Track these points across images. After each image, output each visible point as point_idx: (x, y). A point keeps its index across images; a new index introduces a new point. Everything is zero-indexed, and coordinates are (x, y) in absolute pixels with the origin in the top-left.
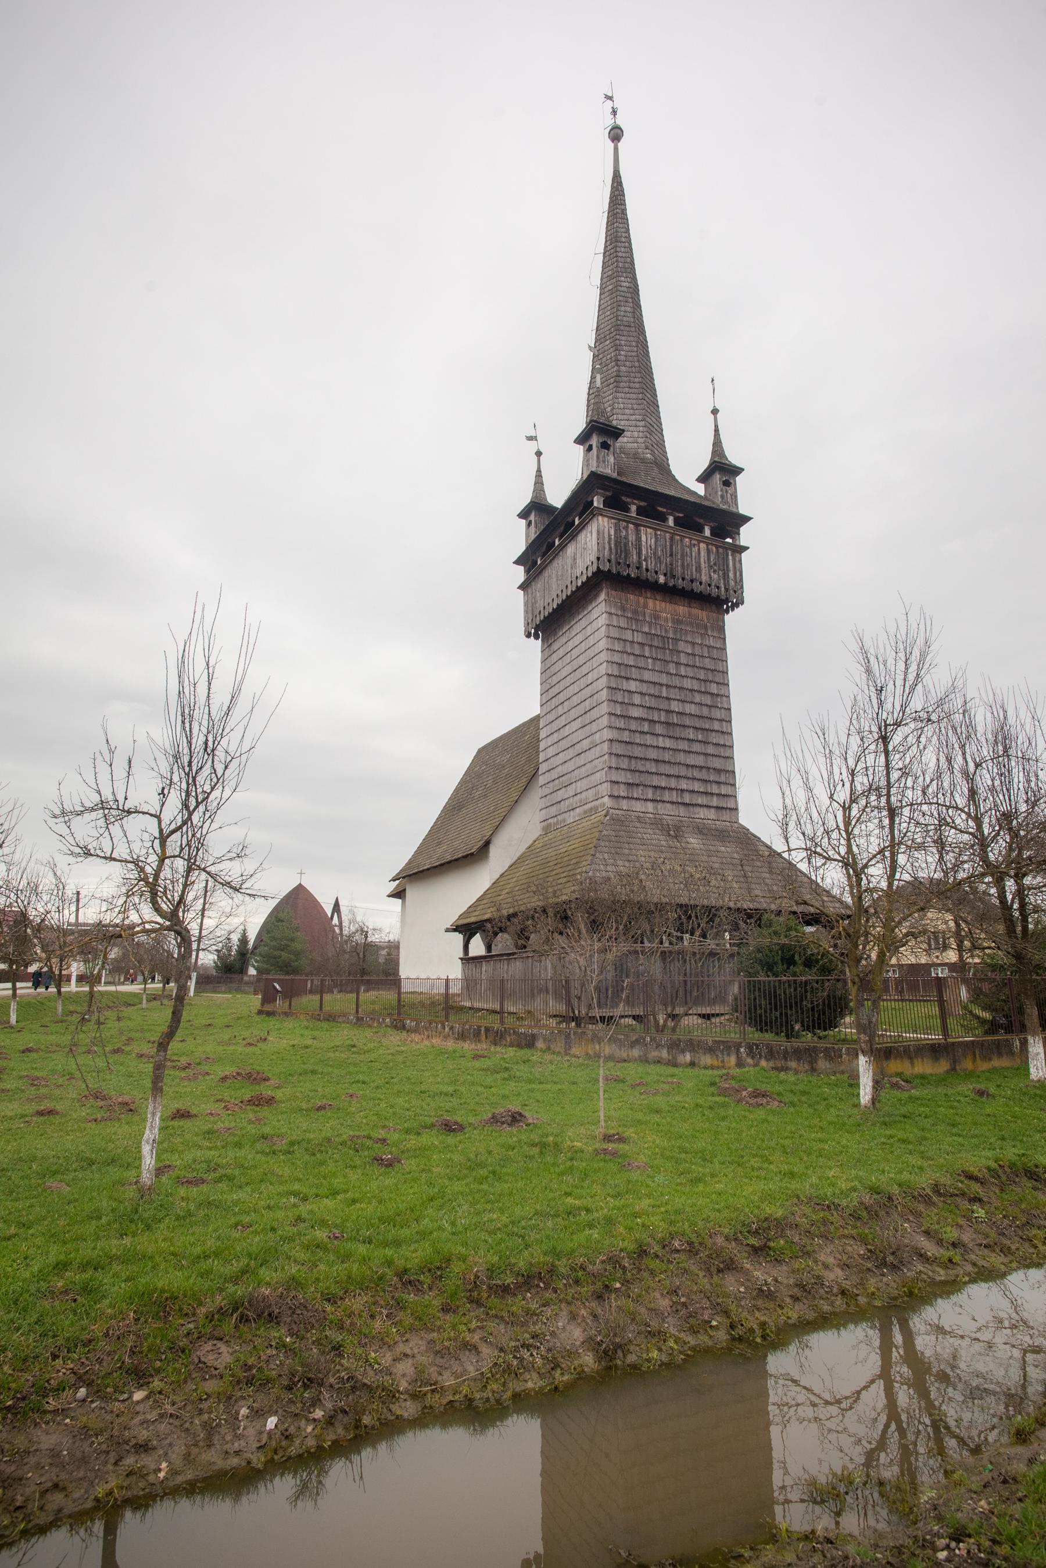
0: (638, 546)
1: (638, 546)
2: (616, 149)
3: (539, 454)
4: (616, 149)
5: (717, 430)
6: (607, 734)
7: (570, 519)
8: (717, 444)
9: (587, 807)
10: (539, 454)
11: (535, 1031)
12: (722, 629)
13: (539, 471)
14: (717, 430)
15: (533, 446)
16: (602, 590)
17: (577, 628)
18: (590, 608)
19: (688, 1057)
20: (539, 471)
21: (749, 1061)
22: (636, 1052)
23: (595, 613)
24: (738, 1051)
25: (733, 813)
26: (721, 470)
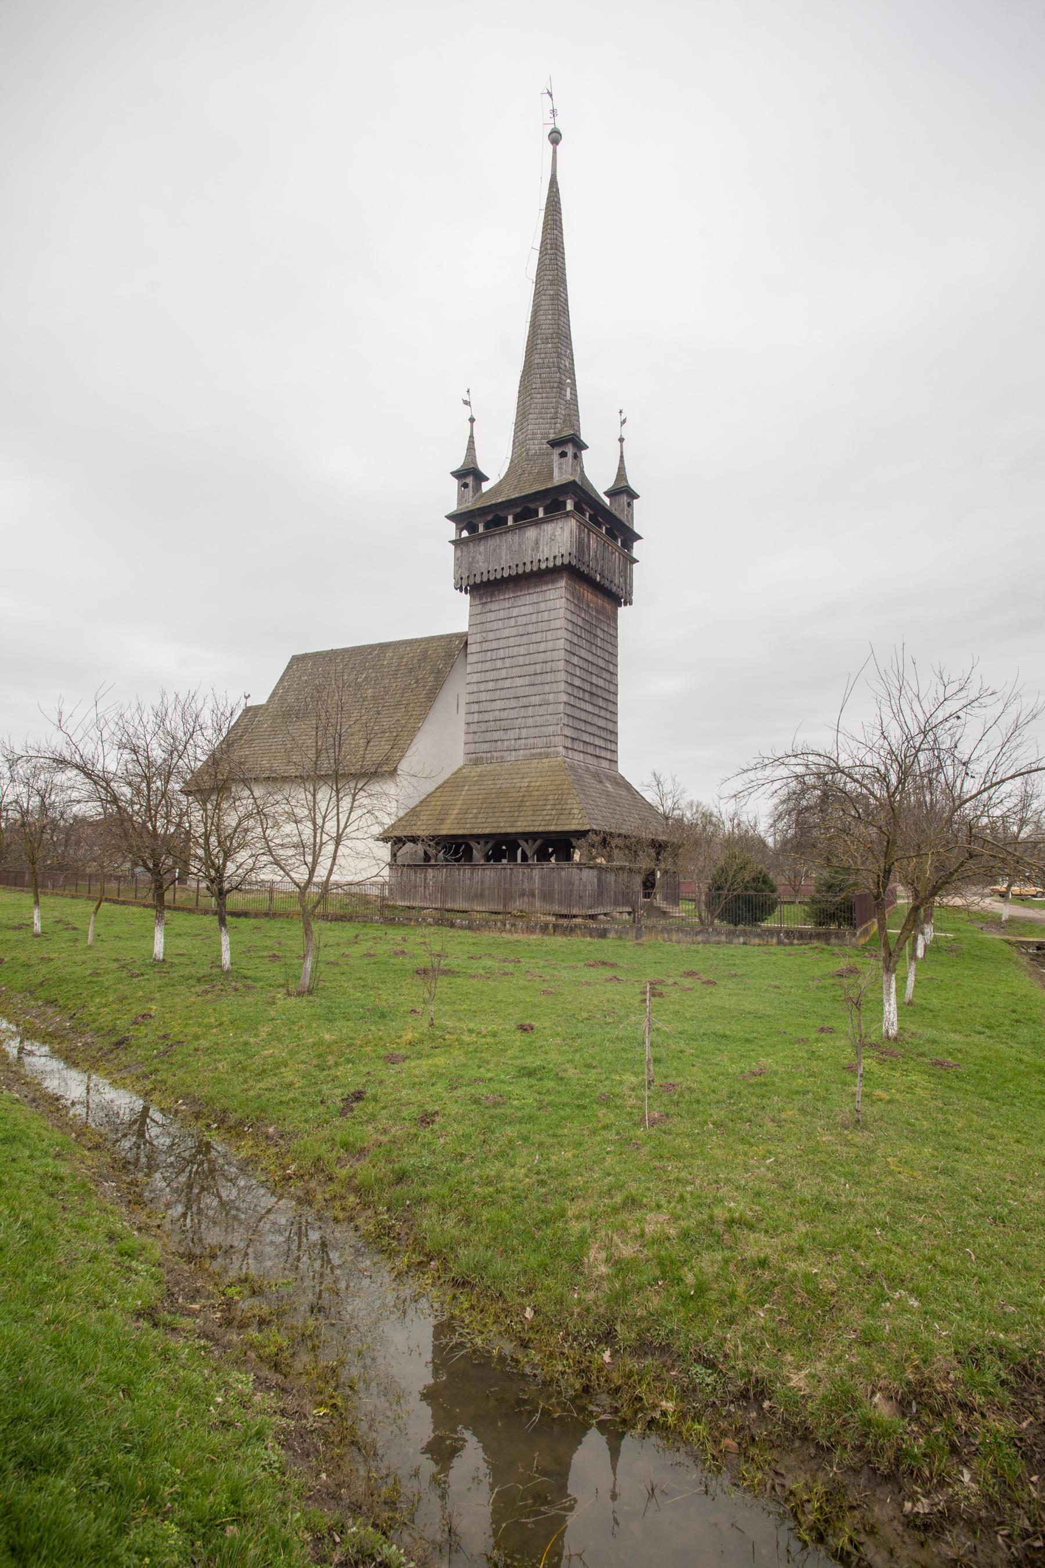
0: (551, 531)
1: (551, 531)
2: (555, 152)
3: (472, 420)
4: (555, 152)
5: (622, 457)
6: (564, 698)
7: (532, 506)
8: (621, 469)
9: (533, 751)
10: (472, 420)
11: (607, 926)
12: (614, 618)
13: (471, 436)
14: (622, 457)
15: (467, 412)
16: (562, 578)
17: (528, 599)
18: (545, 588)
19: (742, 940)
20: (471, 436)
21: (786, 941)
22: (699, 938)
23: (551, 595)
24: (779, 935)
25: (613, 764)
26: (623, 491)
